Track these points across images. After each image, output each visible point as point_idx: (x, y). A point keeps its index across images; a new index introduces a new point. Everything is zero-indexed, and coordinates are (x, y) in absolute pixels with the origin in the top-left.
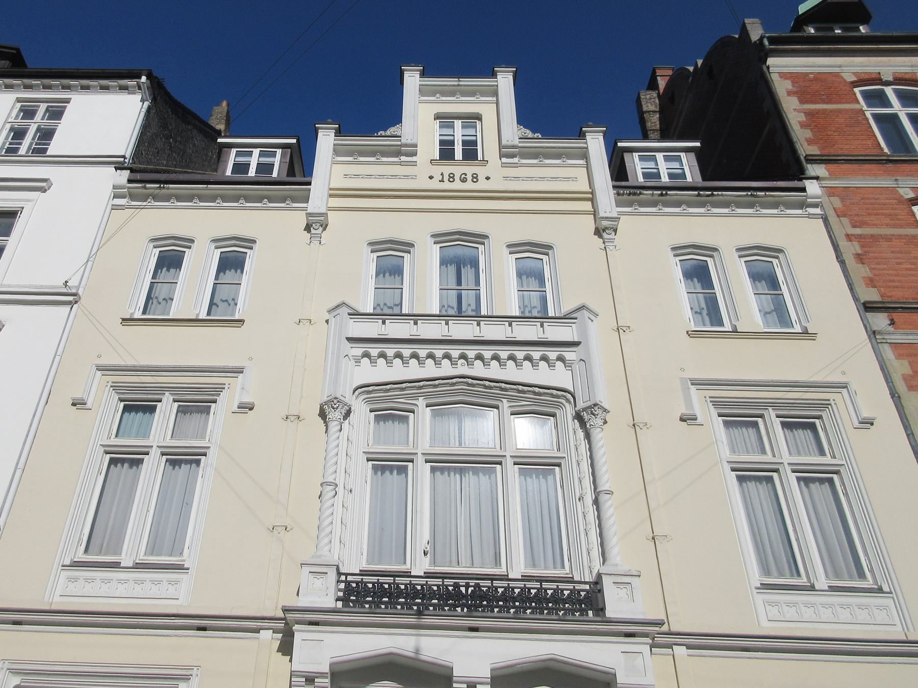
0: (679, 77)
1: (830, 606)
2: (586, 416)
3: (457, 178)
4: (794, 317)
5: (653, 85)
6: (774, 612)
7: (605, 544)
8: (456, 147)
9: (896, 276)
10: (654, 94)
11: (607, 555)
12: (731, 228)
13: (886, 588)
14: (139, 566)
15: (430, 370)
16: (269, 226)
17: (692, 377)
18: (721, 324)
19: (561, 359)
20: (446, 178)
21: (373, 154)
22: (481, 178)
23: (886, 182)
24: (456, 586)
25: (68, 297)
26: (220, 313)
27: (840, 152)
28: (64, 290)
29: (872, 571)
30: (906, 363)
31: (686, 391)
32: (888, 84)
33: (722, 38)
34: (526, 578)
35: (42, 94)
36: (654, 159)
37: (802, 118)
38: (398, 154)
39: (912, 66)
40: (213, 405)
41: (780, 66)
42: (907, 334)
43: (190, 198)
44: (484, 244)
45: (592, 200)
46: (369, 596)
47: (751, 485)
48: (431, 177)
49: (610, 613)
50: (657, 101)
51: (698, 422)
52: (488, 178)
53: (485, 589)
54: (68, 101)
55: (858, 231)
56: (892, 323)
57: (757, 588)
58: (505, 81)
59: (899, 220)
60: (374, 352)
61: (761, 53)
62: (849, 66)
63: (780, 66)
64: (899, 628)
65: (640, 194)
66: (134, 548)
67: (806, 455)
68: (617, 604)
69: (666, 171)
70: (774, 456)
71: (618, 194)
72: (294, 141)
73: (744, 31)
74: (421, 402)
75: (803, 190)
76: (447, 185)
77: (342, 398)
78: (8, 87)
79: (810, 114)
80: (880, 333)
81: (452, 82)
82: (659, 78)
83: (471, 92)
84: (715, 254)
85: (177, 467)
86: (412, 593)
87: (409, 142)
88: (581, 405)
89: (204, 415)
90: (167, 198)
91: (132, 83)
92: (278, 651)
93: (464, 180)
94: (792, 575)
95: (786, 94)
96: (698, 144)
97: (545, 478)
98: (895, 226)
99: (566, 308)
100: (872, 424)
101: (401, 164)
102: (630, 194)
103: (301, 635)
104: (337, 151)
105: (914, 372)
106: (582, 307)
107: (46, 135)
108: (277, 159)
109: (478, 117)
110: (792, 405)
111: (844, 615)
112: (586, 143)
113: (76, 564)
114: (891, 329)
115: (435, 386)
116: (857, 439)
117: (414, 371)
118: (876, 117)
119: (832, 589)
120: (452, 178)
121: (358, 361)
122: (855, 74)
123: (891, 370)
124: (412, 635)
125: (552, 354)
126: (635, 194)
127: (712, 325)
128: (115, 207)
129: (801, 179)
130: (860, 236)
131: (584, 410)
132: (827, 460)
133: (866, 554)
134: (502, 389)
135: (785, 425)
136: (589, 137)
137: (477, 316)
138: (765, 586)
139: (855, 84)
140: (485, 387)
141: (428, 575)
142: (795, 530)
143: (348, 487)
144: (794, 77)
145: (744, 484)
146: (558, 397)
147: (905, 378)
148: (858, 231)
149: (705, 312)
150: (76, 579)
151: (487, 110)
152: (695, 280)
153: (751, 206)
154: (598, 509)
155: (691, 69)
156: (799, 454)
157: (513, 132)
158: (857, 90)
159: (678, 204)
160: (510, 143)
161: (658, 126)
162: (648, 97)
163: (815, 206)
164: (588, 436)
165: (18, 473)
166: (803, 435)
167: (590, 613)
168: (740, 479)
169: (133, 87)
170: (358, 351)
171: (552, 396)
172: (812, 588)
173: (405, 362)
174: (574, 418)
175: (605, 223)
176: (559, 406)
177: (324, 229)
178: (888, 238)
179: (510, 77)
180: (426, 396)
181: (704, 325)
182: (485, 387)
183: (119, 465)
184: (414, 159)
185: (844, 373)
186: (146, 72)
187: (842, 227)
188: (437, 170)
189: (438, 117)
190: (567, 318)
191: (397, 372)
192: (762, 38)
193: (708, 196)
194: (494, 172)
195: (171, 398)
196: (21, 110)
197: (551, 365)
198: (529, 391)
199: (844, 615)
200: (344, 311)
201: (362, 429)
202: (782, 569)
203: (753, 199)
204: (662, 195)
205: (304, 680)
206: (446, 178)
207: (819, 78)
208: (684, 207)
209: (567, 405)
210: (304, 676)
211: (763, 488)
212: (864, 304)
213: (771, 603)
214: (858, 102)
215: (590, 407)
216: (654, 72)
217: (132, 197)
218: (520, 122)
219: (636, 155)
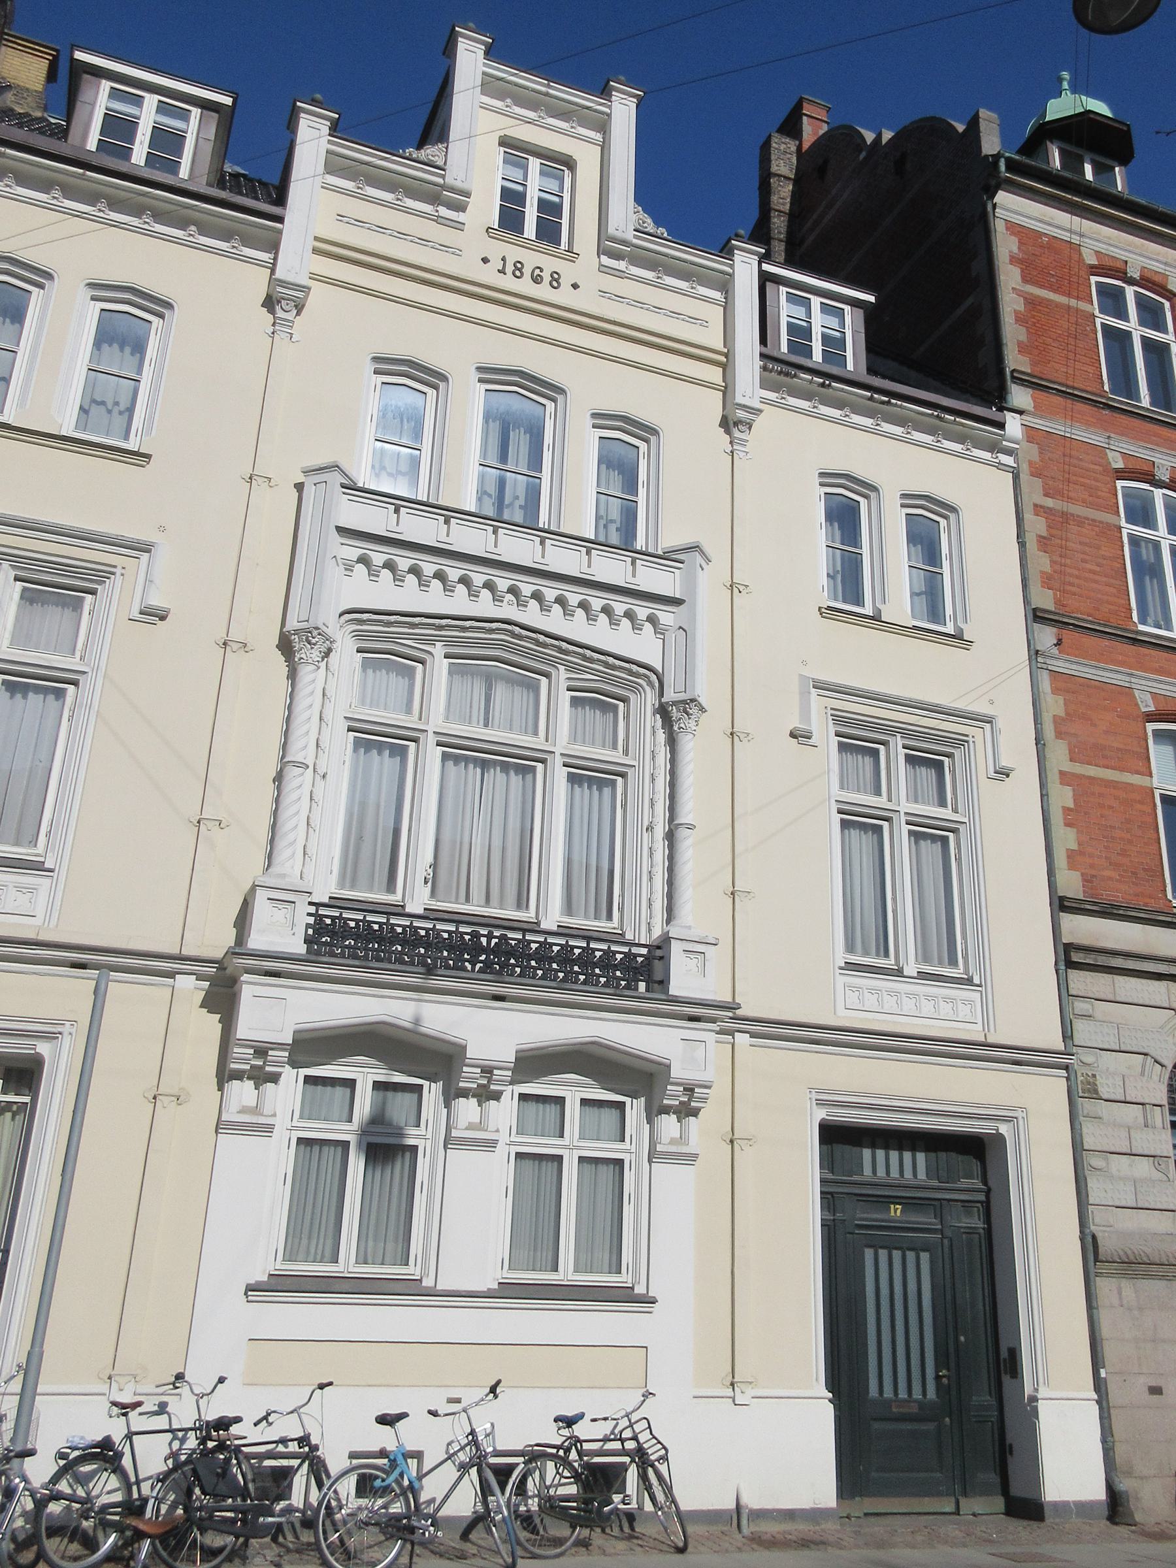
0: (841, 139)
2: (675, 713)
3: (527, 271)
4: (949, 611)
5: (791, 126)
6: (853, 998)
7: (676, 896)
9: (1077, 577)
10: (792, 146)
11: (676, 911)
12: (901, 458)
13: (976, 980)
15: (459, 603)
18: (859, 602)
20: (510, 268)
21: (391, 187)
22: (565, 282)
24: (476, 935)
29: (966, 958)
30: (1061, 700)
31: (804, 695)
32: (1131, 282)
33: (933, 118)
34: (564, 931)
37: (1021, 307)
38: (434, 198)
39: (1166, 264)
41: (1011, 207)
43: (45, 186)
46: (348, 939)
47: (854, 833)
48: (485, 260)
49: (675, 989)
50: (794, 160)
51: (811, 741)
52: (575, 286)
53: (513, 943)
55: (1049, 503)
56: (1059, 643)
57: (841, 968)
58: (623, 110)
59: (1098, 497)
60: (378, 559)
63: (1011, 207)
64: (979, 1027)
65: (795, 376)
67: (923, 803)
68: (685, 978)
69: (820, 329)
70: (890, 800)
71: (765, 368)
72: (228, 101)
74: (439, 650)
75: (1001, 426)
76: (508, 282)
77: (324, 629)
79: (1032, 303)
81: (535, 83)
82: (805, 118)
83: (565, 113)
84: (873, 495)
87: (459, 184)
88: (670, 696)
92: (201, 1006)
94: (878, 955)
95: (1007, 260)
99: (668, 540)
100: (1008, 776)
101: (439, 220)
102: (780, 373)
104: (333, 165)
105: (1067, 714)
106: (695, 548)
109: (569, 163)
114: (1055, 651)
117: (434, 600)
119: (922, 975)
120: (518, 268)
121: (349, 568)
124: (411, 1000)
125: (642, 612)
126: (787, 374)
127: (844, 601)
129: (1001, 409)
130: (1050, 509)
131: (675, 703)
132: (946, 813)
133: (964, 937)
135: (909, 759)
136: (739, 256)
137: (530, 525)
138: (850, 966)
139: (1096, 270)
142: (894, 899)
143: (321, 771)
145: (846, 831)
146: (637, 675)
148: (1049, 503)
152: (836, 525)
155: (869, 137)
156: (916, 801)
157: (625, 215)
158: (1094, 279)
159: (839, 405)
160: (619, 234)
161: (788, 207)
163: (1009, 452)
164: (672, 741)
166: (926, 775)
168: (845, 824)
170: (352, 551)
172: (899, 973)
173: (423, 583)
175: (741, 414)
176: (636, 689)
177: (298, 314)
178: (1080, 521)
179: (632, 104)
180: (449, 642)
181: (836, 599)
185: (992, 702)
187: (1034, 492)
190: (670, 557)
191: (408, 597)
192: (997, 157)
193: (883, 403)
195: (12, 573)
197: (636, 627)
198: (599, 660)
200: (336, 479)
201: (341, 683)
202: (869, 944)
203: (937, 422)
204: (823, 385)
205: (252, 1051)
208: (847, 411)
209: (648, 689)
210: (252, 1047)
211: (868, 839)
212: (1035, 610)
213: (851, 987)
215: (684, 702)
216: (798, 107)
218: (638, 199)
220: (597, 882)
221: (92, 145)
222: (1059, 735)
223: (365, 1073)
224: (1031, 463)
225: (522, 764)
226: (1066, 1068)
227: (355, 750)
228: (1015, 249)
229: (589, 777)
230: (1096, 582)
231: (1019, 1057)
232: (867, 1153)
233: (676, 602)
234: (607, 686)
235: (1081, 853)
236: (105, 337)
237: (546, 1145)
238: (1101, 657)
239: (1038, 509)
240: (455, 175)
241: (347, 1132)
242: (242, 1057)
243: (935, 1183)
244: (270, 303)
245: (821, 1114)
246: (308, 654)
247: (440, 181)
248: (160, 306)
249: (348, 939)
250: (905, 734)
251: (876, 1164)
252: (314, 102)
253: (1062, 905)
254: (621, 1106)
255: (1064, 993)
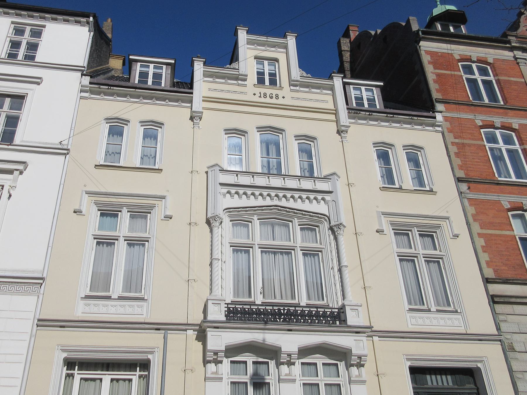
0: (364, 35)
1: (437, 318)
3: (268, 96)
4: (426, 182)
5: (346, 35)
6: (413, 321)
8: (265, 77)
10: (348, 40)
11: (346, 296)
12: (400, 134)
13: (459, 311)
14: (120, 298)
15: (260, 202)
16: (171, 114)
17: (382, 211)
18: (394, 184)
19: (323, 199)
20: (262, 95)
21: (223, 78)
23: (471, 116)
24: (279, 310)
25: (62, 151)
26: (149, 165)
27: (451, 98)
28: (60, 147)
29: (453, 303)
32: (474, 62)
33: (394, 23)
35: (29, 21)
36: (360, 89)
37: (434, 77)
38: (237, 79)
40: (149, 215)
42: (475, 194)
44: (282, 134)
45: (336, 114)
46: (240, 314)
47: (405, 263)
48: (254, 94)
49: (349, 323)
54: (44, 26)
55: (457, 141)
56: (469, 188)
58: (291, 41)
60: (233, 191)
61: (416, 38)
62: (459, 50)
63: (427, 46)
66: (117, 288)
68: (352, 319)
69: (366, 97)
70: (416, 250)
71: (349, 113)
72: (173, 62)
73: (408, 22)
74: (255, 217)
76: (263, 100)
78: (5, 13)
79: (438, 75)
80: (464, 193)
81: (263, 38)
84: (392, 148)
85: (132, 247)
86: (259, 313)
87: (243, 73)
88: (333, 223)
89: (116, 218)
90: (112, 95)
91: (84, 20)
93: (271, 98)
94: (420, 305)
96: (382, 84)
97: (314, 257)
98: (473, 139)
99: (325, 173)
101: (238, 85)
102: (354, 113)
103: (211, 334)
107: (33, 47)
108: (165, 72)
109: (277, 60)
110: (424, 226)
111: (442, 322)
112: (333, 82)
113: (87, 297)
114: (468, 191)
115: (263, 210)
116: (451, 243)
117: (252, 202)
118: (467, 79)
119: (438, 311)
120: (265, 95)
121: (224, 196)
122: (459, 55)
123: (467, 210)
125: (320, 197)
126: (357, 113)
128: (82, 98)
130: (458, 143)
133: (452, 296)
134: (294, 213)
138: (411, 310)
140: (287, 211)
141: (263, 304)
142: (423, 284)
144: (431, 54)
146: (321, 218)
147: (473, 215)
148: (457, 141)
149: (385, 176)
150: (89, 305)
151: (282, 57)
152: (381, 159)
153: (410, 123)
154: (341, 274)
155: (373, 33)
157: (297, 73)
158: (460, 64)
159: (376, 120)
160: (295, 79)
162: (345, 41)
164: (336, 238)
165: (50, 249)
166: (428, 240)
167: (338, 323)
168: (401, 260)
169: (84, 22)
170: (225, 190)
171: (318, 217)
172: (429, 310)
174: (329, 229)
175: (343, 128)
176: (321, 222)
178: (469, 145)
180: (258, 215)
182: (287, 211)
183: (101, 245)
184: (245, 83)
185: (447, 212)
186: (92, 15)
187: (450, 138)
188: (257, 90)
189: (256, 58)
190: (326, 178)
191: (244, 202)
192: (418, 31)
193: (391, 117)
194: (286, 94)
196: (14, 29)
197: (318, 202)
199: (442, 322)
200: (218, 168)
201: (226, 232)
202: (417, 301)
204: (370, 115)
206: (262, 95)
207: (443, 55)
209: (325, 222)
211: (410, 264)
212: (458, 178)
214: (460, 71)
215: (338, 225)
217: (92, 92)
218: (300, 67)
219: (139, 64)
220: (317, 288)
221: (137, 82)
222: (475, 220)
223: (250, 359)
224: (447, 128)
225: (287, 251)
226: (500, 341)
227: (233, 253)
228: (430, 59)
229: (308, 253)
230: (479, 165)
231: (480, 338)
232: (428, 377)
233: (331, 192)
234: (311, 223)
235: (491, 261)
236: (146, 136)
237: (313, 380)
238: (485, 191)
239: (453, 143)
240: (242, 71)
241: (246, 379)
242: (210, 356)
243: (456, 387)
244: (192, 119)
245: (65, 355)
246: (215, 224)
247: (238, 73)
248: (160, 125)
249: (240, 314)
250: (417, 226)
251: (432, 381)
252: (198, 57)
253: (487, 281)
254: (267, 363)
255: (494, 313)
